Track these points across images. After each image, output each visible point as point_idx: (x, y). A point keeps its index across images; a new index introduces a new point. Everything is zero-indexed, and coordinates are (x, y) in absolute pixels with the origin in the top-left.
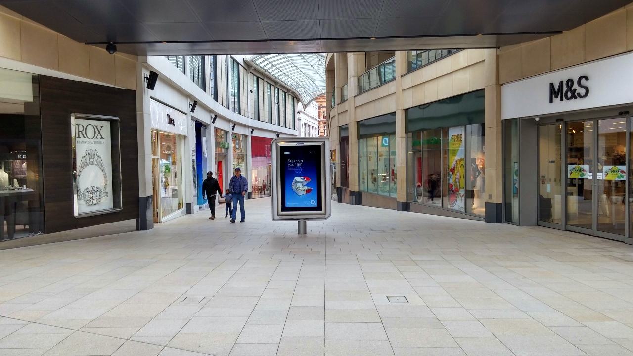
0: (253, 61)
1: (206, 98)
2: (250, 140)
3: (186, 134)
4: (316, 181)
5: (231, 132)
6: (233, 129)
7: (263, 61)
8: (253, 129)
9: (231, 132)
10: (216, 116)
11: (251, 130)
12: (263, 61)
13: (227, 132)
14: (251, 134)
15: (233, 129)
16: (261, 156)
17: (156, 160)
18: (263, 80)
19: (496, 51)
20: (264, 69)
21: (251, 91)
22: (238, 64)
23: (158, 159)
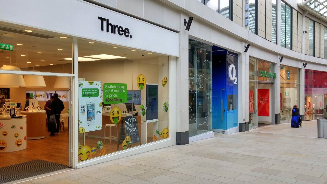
0: (307, 6)
1: (258, 40)
2: (303, 72)
3: (177, 55)
4: (77, 47)
5: (279, 64)
6: (281, 62)
7: (323, 8)
8: (306, 63)
9: (279, 64)
10: (191, 19)
11: (305, 64)
12: (323, 8)
13: (274, 64)
14: (305, 67)
15: (281, 62)
16: (321, 86)
17: (71, 78)
18: (320, 24)
19: (319, 122)
20: (320, 14)
21: (306, 32)
22: (292, 8)
23: (74, 77)
